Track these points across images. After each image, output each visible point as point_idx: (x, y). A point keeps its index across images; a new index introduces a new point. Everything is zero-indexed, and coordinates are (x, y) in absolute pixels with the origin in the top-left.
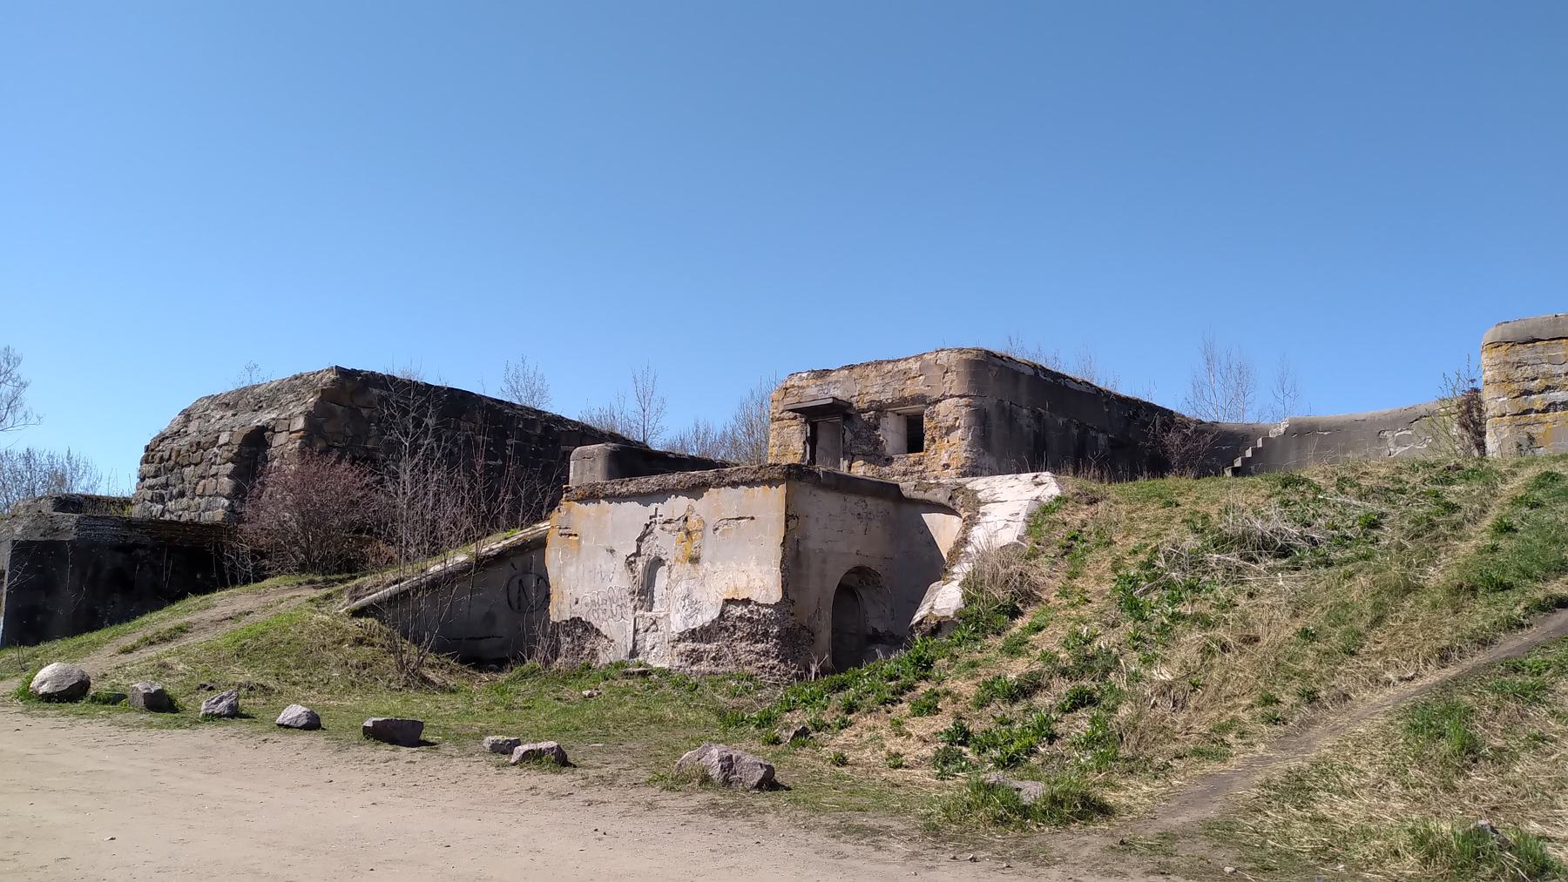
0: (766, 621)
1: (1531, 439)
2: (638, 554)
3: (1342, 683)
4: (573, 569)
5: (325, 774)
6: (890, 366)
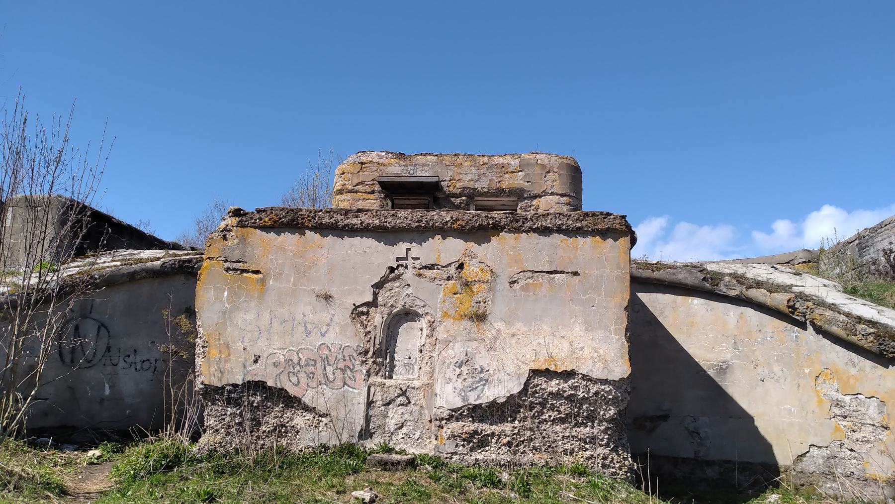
2: (374, 304)
4: (250, 316)
6: (485, 159)
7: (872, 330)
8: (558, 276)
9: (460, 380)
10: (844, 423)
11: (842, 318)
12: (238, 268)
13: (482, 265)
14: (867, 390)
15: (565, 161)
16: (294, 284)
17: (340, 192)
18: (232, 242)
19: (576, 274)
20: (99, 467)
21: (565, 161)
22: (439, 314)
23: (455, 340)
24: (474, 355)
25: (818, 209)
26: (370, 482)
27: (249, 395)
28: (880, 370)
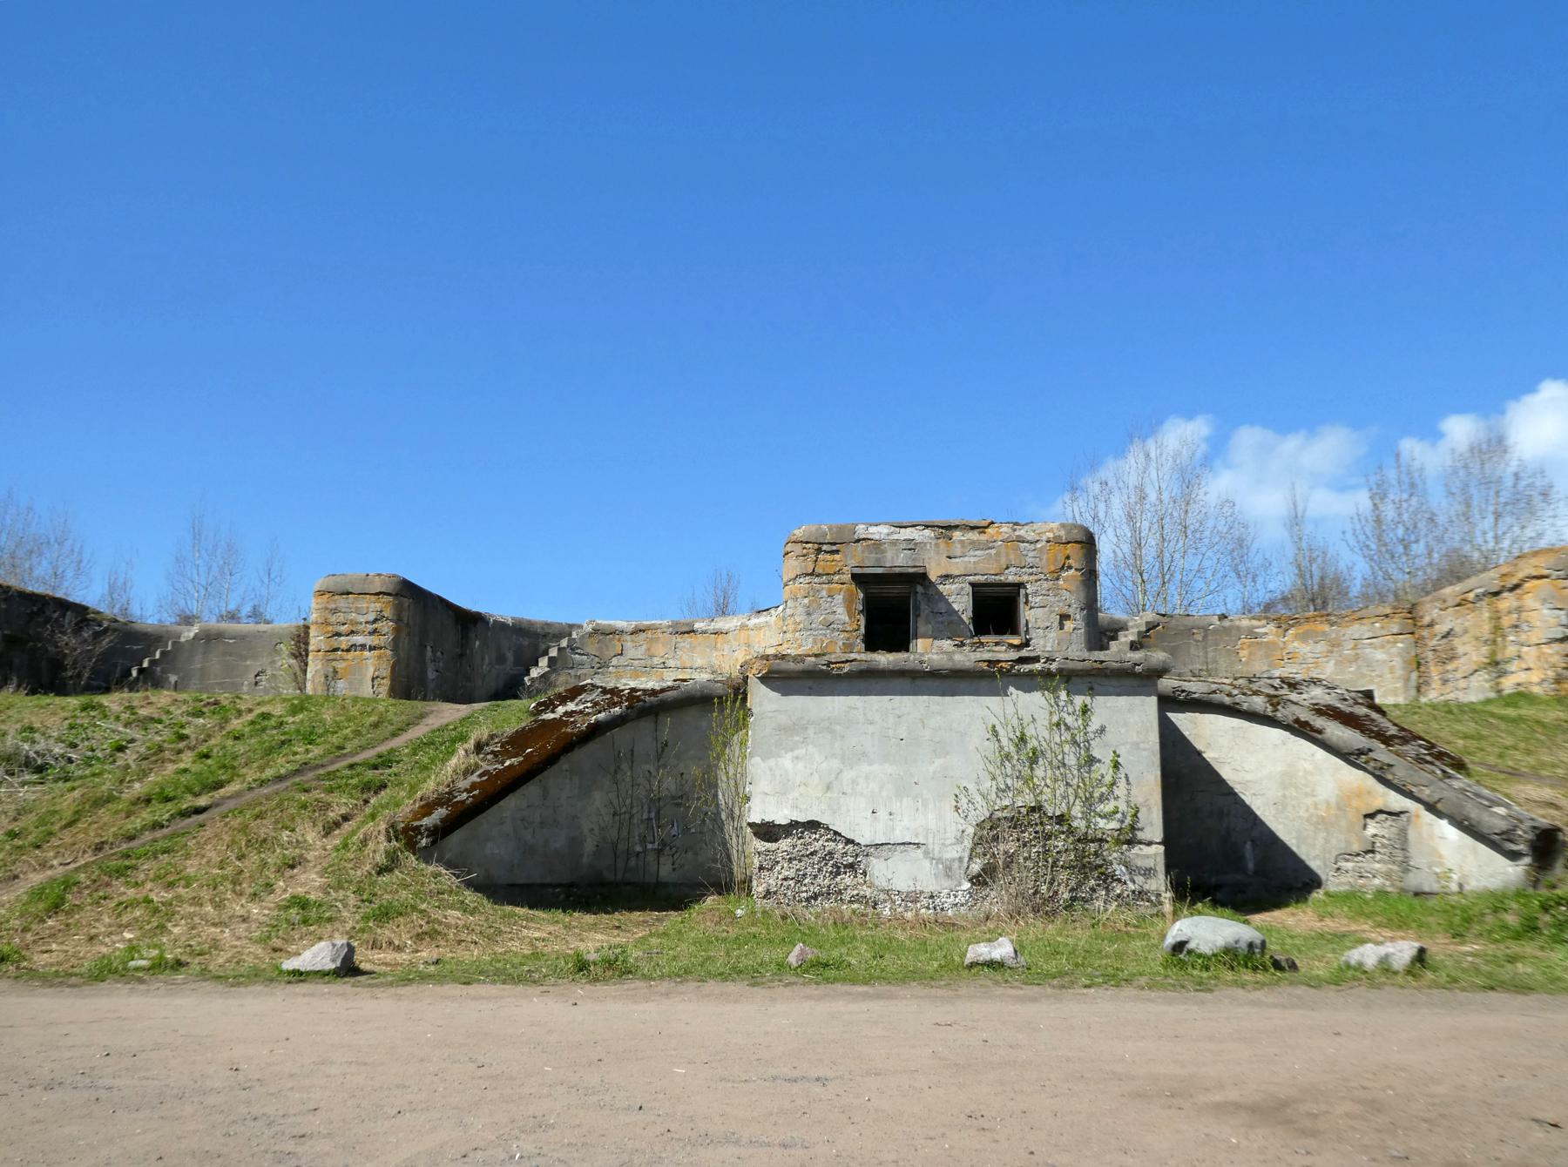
1: (335, 672)
3: (17, 868)
5: (823, 660)
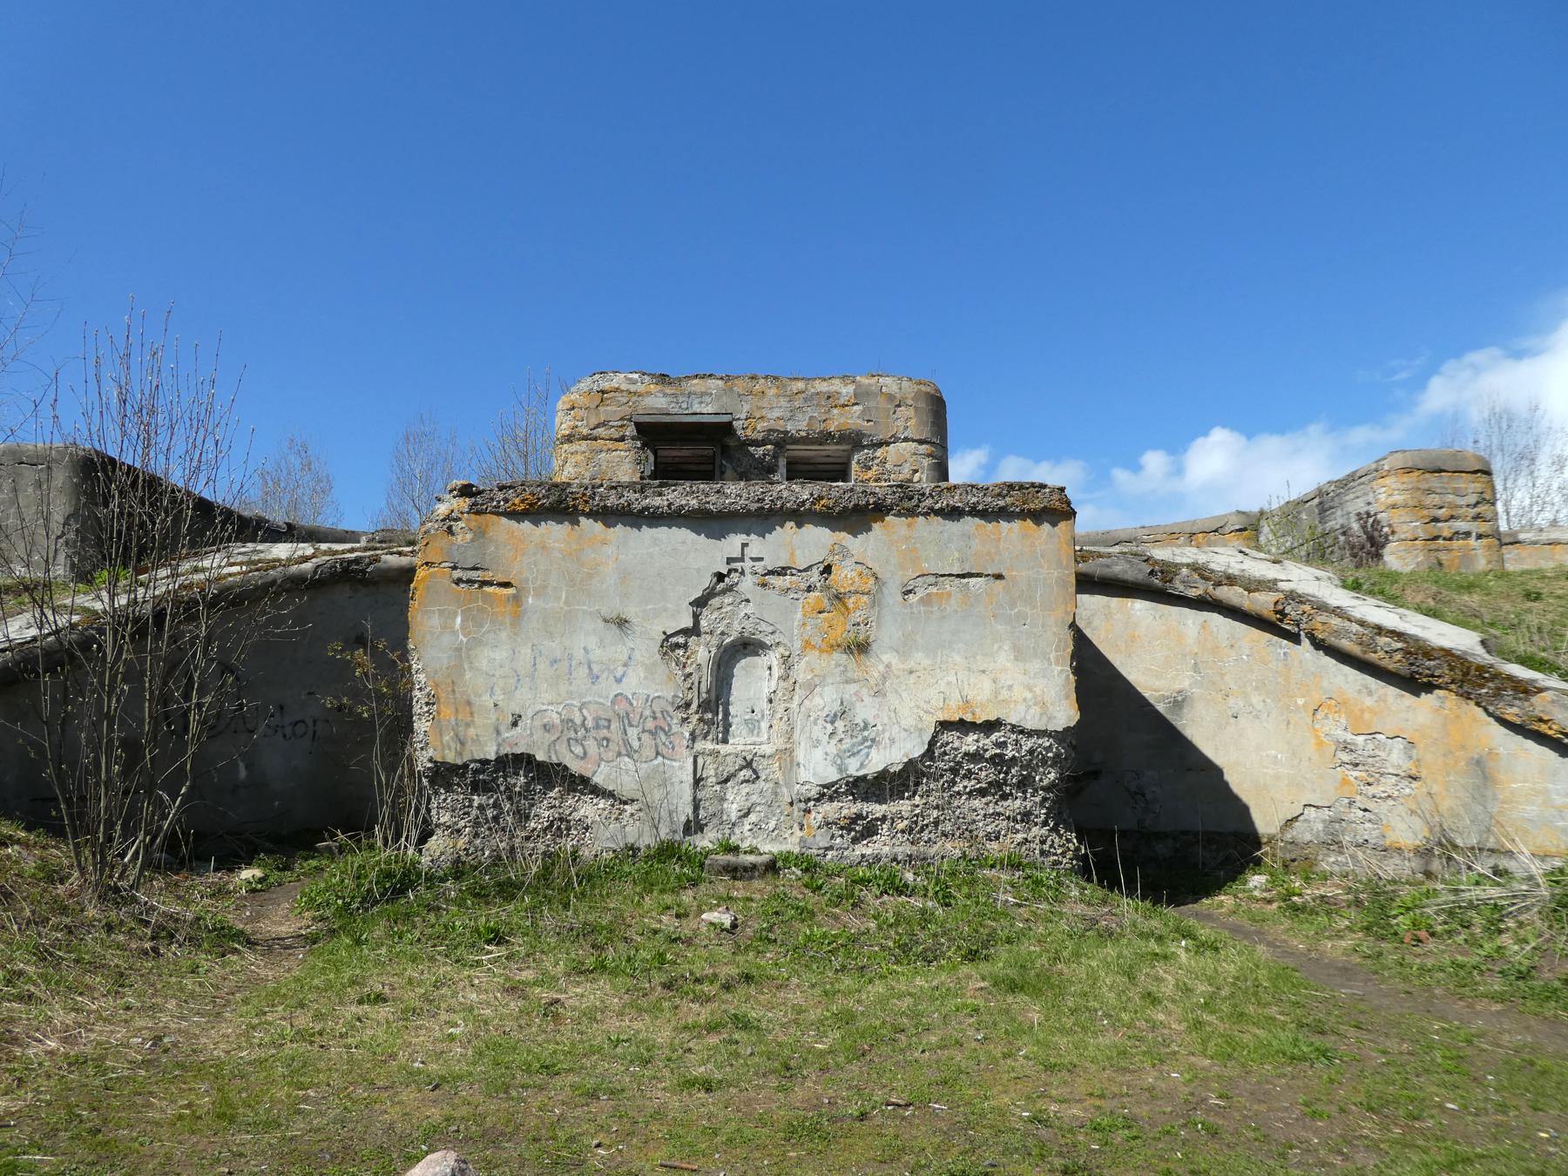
0: (1034, 760)
2: (694, 631)
4: (501, 655)
6: (800, 385)
7: (1400, 645)
8: (973, 581)
9: (834, 742)
10: (1355, 774)
11: (1355, 627)
12: (476, 579)
13: (859, 568)
14: (1390, 727)
15: (923, 388)
16: (566, 603)
17: (569, 439)
18: (462, 538)
19: (999, 577)
20: (267, 896)
21: (923, 388)
22: (798, 644)
23: (823, 683)
24: (852, 704)
25: (1206, 433)
26: (720, 898)
27: (505, 777)
28: (1408, 699)
